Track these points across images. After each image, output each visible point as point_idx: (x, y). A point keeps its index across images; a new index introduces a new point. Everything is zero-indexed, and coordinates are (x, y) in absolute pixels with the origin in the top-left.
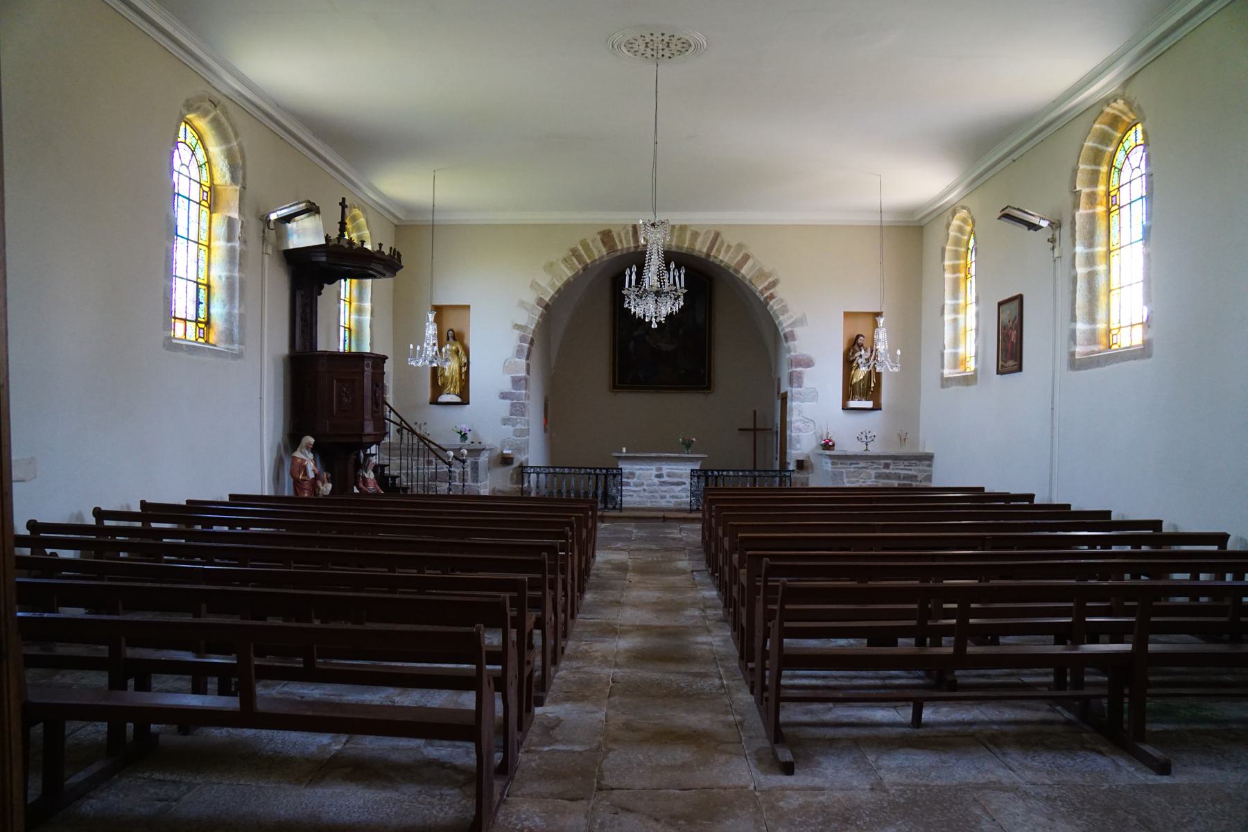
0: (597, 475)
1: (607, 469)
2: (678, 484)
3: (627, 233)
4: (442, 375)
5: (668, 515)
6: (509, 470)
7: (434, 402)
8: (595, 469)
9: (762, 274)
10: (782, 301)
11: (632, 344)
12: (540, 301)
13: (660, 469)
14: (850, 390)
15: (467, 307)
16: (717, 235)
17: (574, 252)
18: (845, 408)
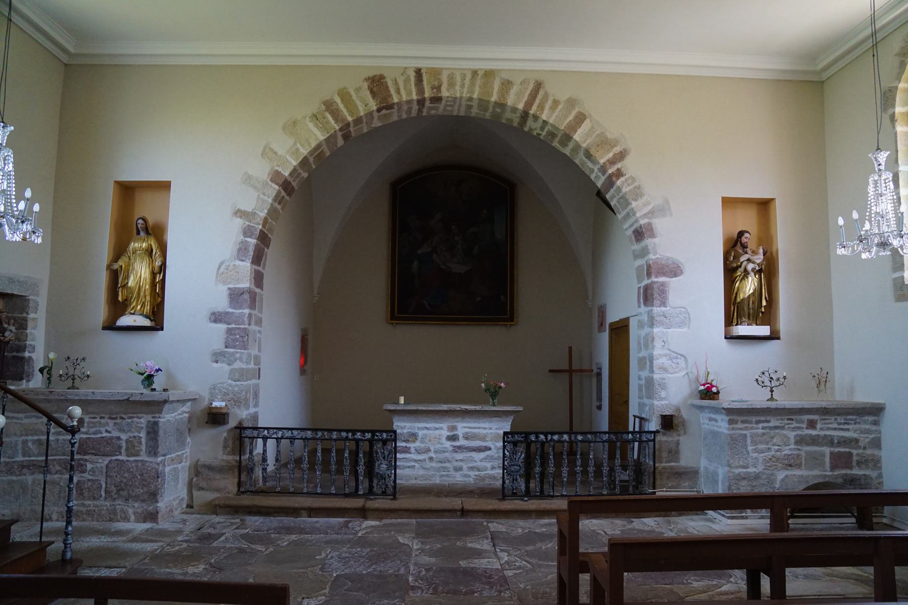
0: (357, 441)
1: (373, 432)
2: (479, 450)
3: (407, 81)
4: (125, 286)
5: (471, 504)
6: (222, 432)
7: (110, 326)
8: (354, 432)
9: (605, 143)
10: (634, 180)
11: (415, 264)
12: (275, 176)
13: (454, 428)
14: (735, 311)
15: (165, 186)
16: (538, 86)
17: (329, 106)
18: (729, 337)
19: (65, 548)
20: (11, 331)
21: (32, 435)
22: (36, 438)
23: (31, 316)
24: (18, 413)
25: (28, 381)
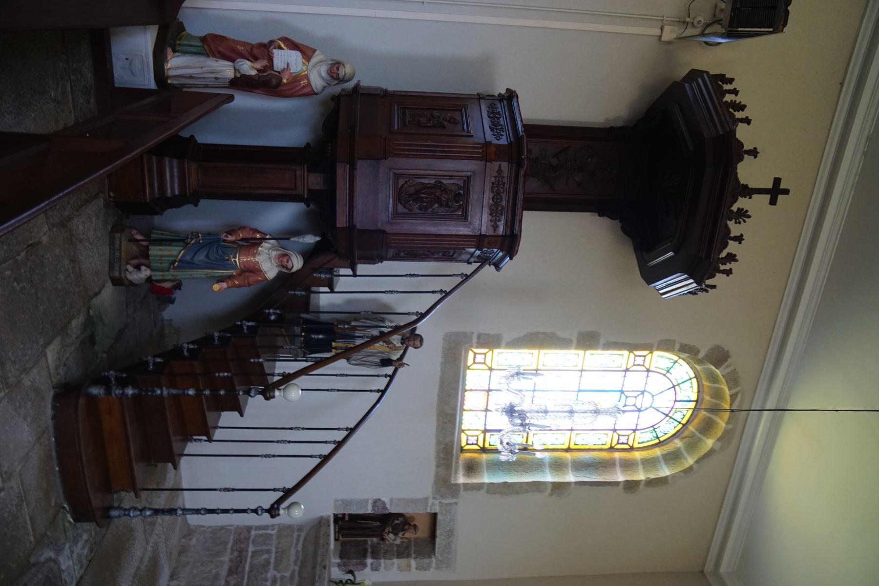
19: (125, 510)
20: (395, 540)
21: (276, 557)
22: (272, 561)
23: (413, 563)
24: (304, 545)
25: (339, 565)
